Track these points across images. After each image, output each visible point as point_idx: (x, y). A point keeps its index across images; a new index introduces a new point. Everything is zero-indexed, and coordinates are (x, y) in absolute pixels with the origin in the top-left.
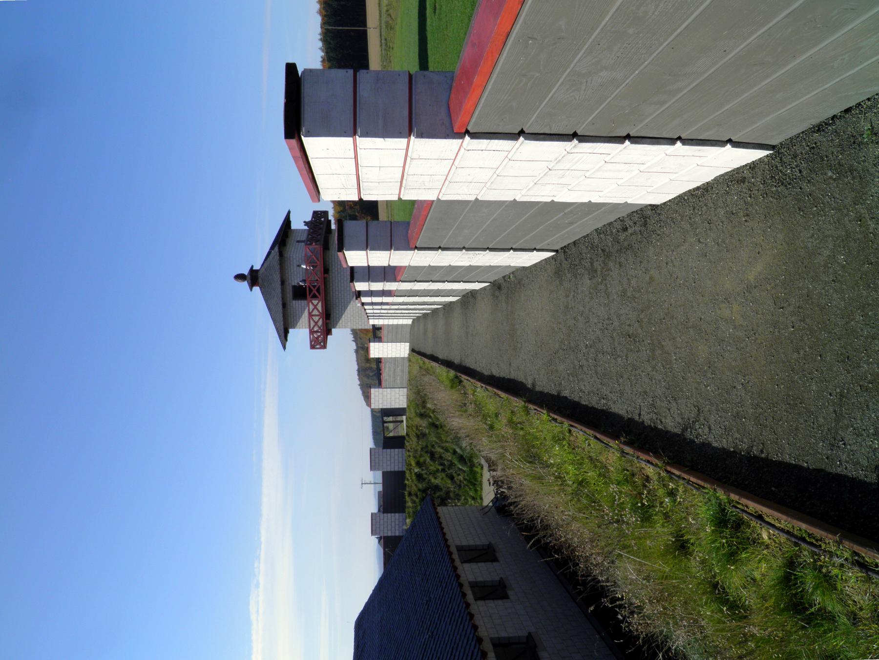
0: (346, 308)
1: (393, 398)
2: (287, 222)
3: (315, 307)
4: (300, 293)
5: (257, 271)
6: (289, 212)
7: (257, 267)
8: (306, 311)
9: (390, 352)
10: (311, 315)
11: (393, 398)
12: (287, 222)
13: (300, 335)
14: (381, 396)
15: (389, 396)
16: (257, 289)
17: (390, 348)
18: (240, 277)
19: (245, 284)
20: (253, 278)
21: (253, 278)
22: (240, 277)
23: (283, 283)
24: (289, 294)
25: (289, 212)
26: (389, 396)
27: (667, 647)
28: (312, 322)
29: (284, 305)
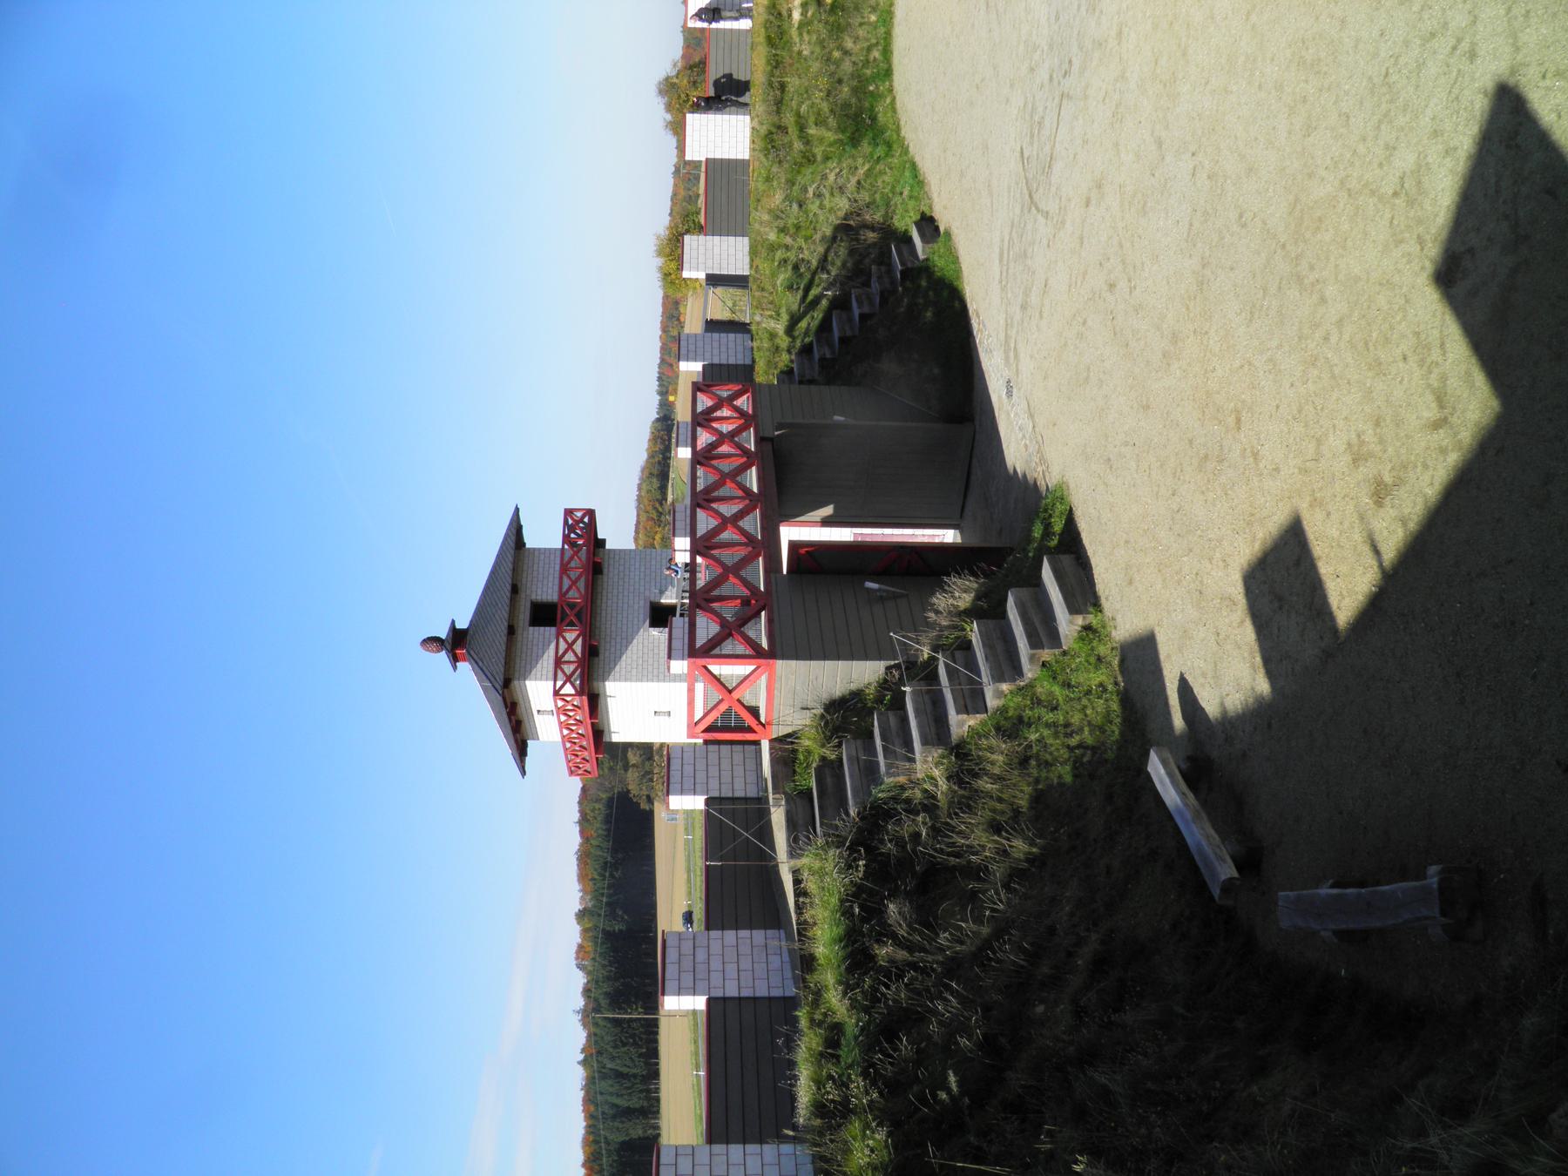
0: (629, 642)
1: (724, 256)
2: (516, 530)
3: (570, 646)
4: (544, 615)
5: (463, 632)
6: (517, 510)
7: (463, 624)
8: (553, 646)
9: (724, 265)
10: (558, 662)
11: (724, 256)
12: (516, 530)
13: (545, 535)
14: (702, 249)
15: (717, 250)
16: (464, 666)
17: (725, 247)
18: (432, 642)
19: (443, 656)
20: (456, 643)
21: (456, 643)
22: (432, 642)
23: (515, 590)
24: (524, 614)
25: (517, 510)
26: (717, 250)
27: (1044, 639)
28: (560, 674)
29: (511, 630)
